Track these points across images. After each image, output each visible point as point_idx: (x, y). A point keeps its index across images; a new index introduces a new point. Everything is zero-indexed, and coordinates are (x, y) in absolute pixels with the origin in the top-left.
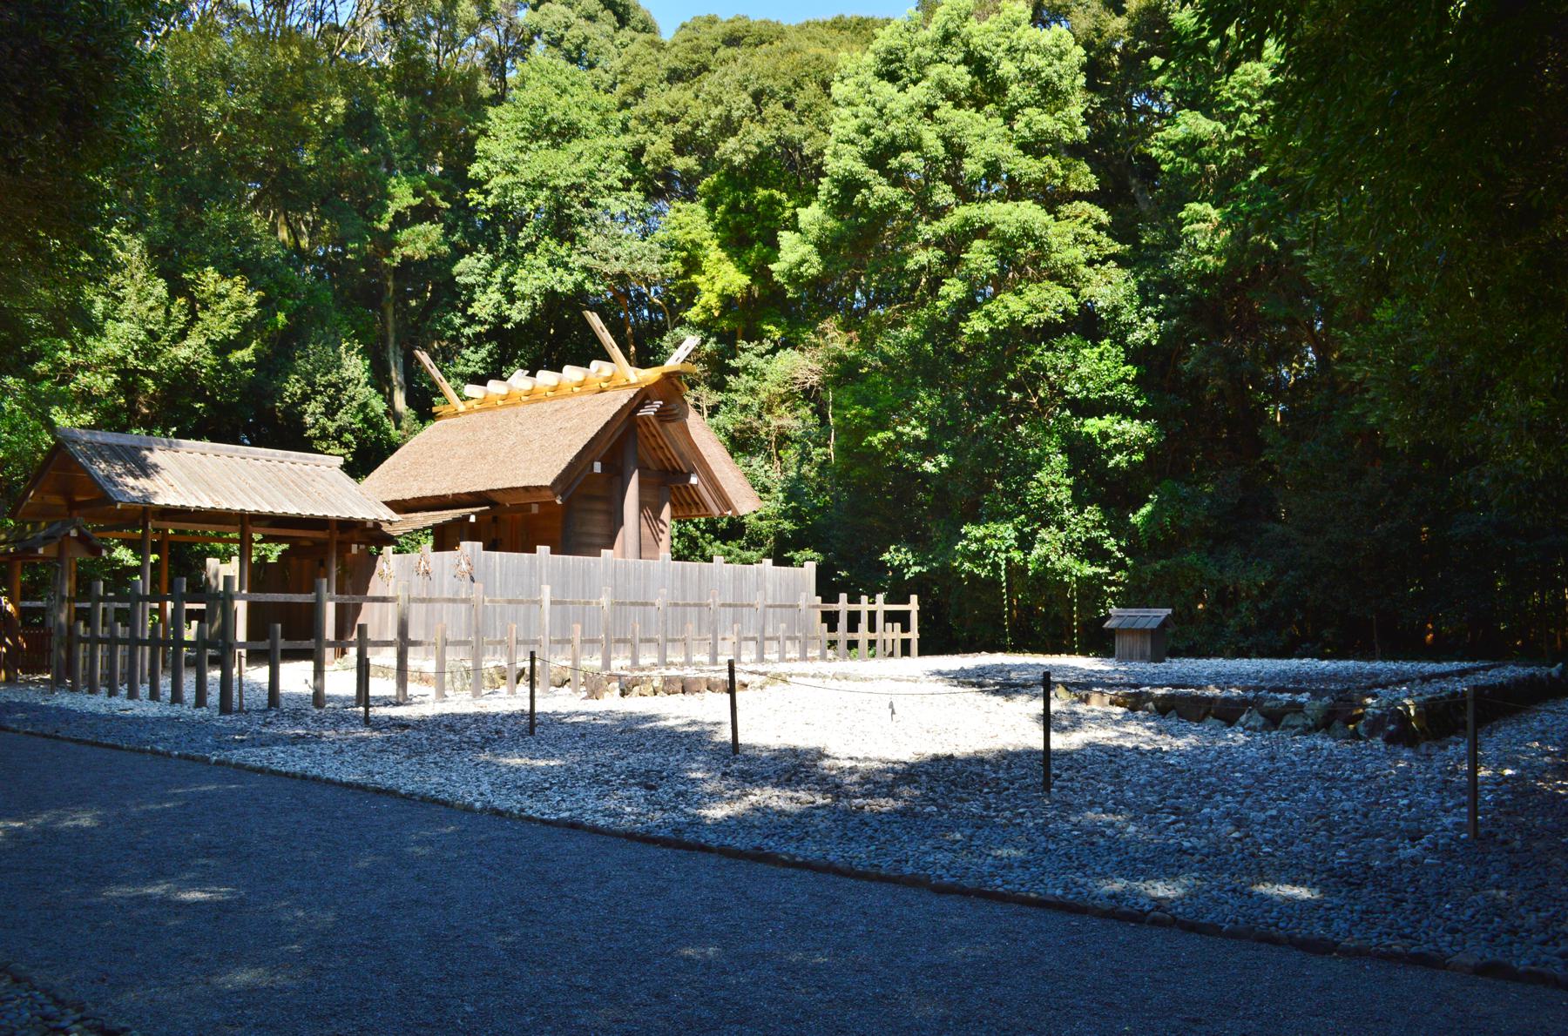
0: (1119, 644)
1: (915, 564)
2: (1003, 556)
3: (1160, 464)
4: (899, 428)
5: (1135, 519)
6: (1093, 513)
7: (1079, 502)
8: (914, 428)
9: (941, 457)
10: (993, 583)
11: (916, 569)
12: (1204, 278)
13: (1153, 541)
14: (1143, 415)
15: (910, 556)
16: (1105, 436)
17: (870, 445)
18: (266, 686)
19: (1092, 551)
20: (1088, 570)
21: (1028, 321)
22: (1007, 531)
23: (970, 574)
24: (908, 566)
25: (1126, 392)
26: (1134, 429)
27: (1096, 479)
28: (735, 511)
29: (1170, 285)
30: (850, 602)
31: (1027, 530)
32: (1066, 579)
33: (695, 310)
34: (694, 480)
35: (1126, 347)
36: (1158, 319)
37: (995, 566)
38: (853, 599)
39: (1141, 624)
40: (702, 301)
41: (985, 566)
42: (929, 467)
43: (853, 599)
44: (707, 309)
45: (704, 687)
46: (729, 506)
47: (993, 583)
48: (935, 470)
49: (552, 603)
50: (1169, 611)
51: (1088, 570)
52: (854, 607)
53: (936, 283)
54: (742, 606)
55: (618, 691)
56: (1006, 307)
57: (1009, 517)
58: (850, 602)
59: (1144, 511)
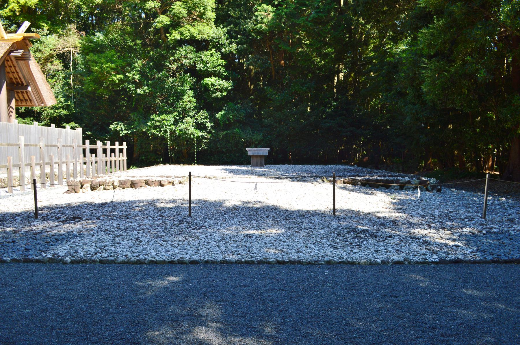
0: (252, 161)
1: (125, 130)
2: (169, 127)
3: (231, 97)
4: (127, 74)
5: (218, 116)
6: (203, 113)
7: (198, 109)
8: (134, 75)
9: (145, 88)
10: (163, 139)
11: (126, 132)
12: (259, 32)
13: (225, 124)
14: (226, 79)
15: (122, 126)
16: (213, 85)
17: (113, 80)
18: (34, 209)
19: (200, 126)
20: (200, 134)
21: (198, 38)
22: (171, 118)
23: (153, 134)
24: (122, 130)
25: (222, 70)
26: (226, 84)
27: (205, 99)
28: (45, 104)
29: (246, 33)
30: (111, 145)
31: (178, 118)
32: (192, 137)
33: (6, 10)
34: (29, 89)
35: (222, 53)
36: (237, 44)
37: (166, 131)
38: (113, 144)
39: (261, 154)
40: (10, 7)
41: (161, 131)
42: (139, 91)
43: (113, 144)
44: (13, 11)
45: (143, 184)
46: (42, 101)
47: (163, 139)
48: (142, 93)
49: (26, 145)
50: (269, 149)
51: (200, 134)
52: (121, 147)
53: (155, 15)
54: (31, 145)
55: (89, 188)
56: (189, 30)
57: (170, 113)
58: (111, 145)
59: (220, 113)
